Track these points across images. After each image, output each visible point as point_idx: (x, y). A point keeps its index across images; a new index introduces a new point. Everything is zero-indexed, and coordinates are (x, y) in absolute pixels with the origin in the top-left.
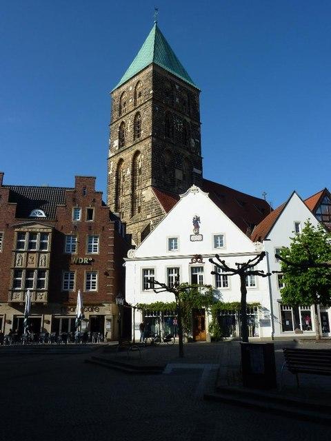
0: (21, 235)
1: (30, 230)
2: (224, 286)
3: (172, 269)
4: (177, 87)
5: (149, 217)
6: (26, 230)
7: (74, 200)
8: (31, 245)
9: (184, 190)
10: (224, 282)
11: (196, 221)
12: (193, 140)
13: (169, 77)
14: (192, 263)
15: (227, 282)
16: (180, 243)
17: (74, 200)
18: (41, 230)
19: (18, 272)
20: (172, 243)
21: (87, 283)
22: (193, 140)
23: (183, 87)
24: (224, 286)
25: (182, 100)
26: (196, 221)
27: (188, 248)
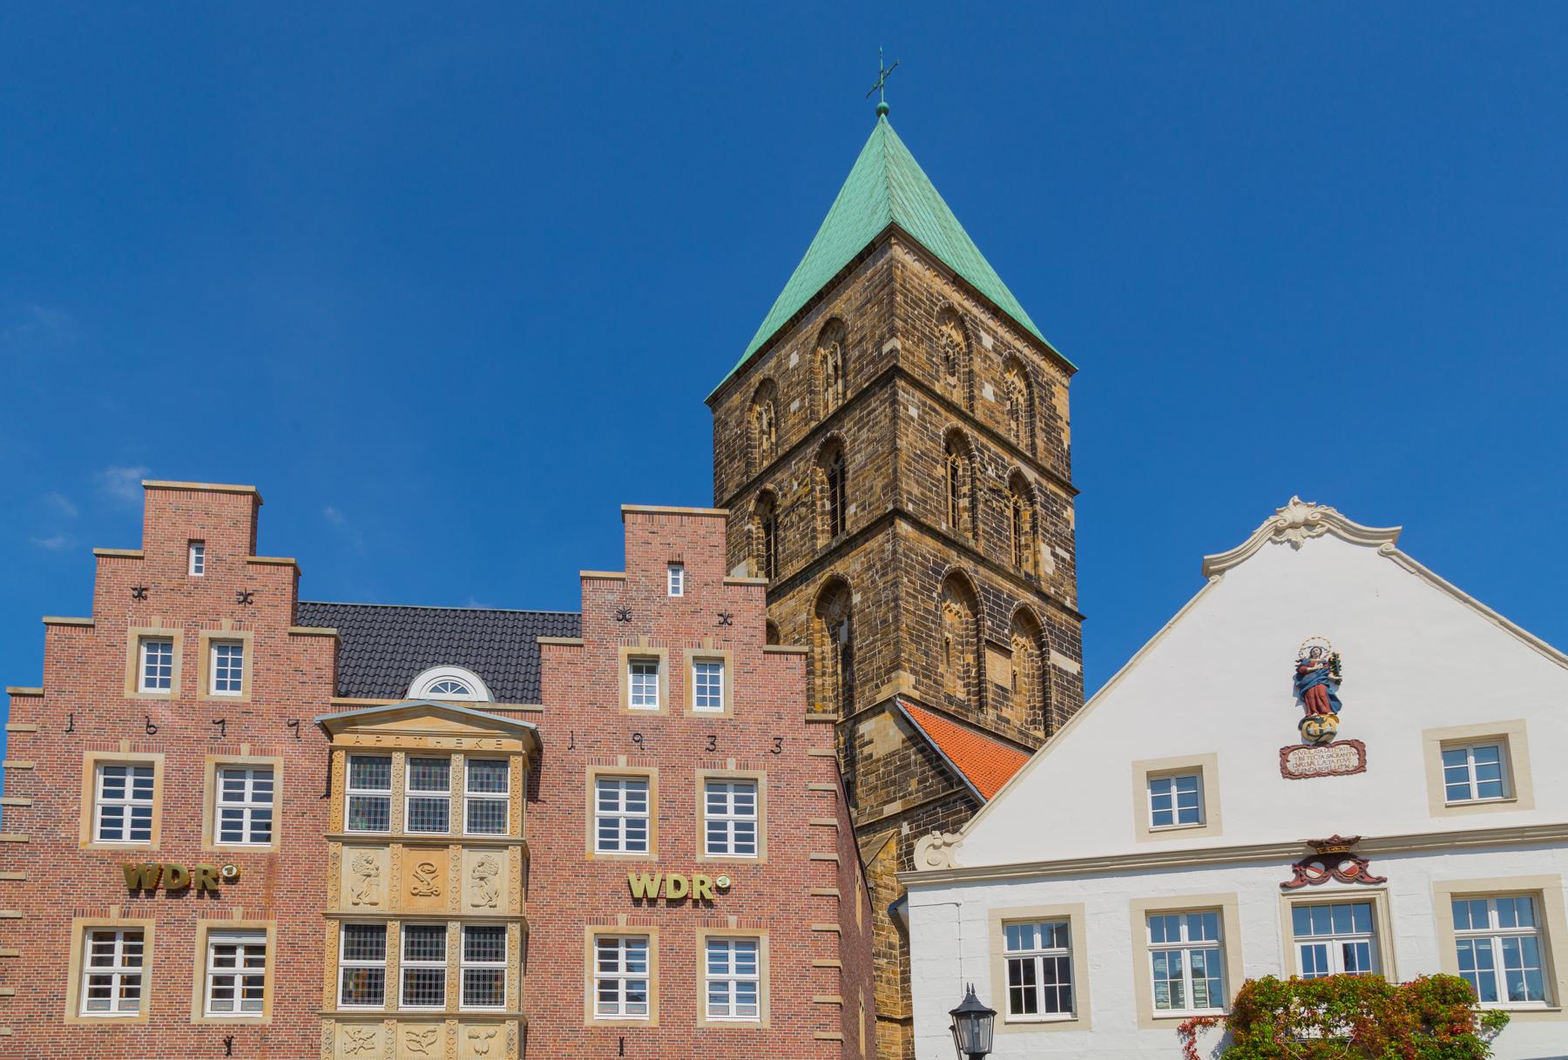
0: (372, 765)
2: (1051, 1007)
3: (1064, 940)
4: (988, 341)
5: (895, 808)
6: (388, 741)
8: (429, 814)
9: (1234, 529)
10: (1030, 979)
11: (1316, 685)
12: (1045, 550)
14: (1302, 879)
15: (1014, 979)
16: (1220, 793)
18: (468, 744)
19: (365, 935)
20: (1178, 790)
21: (604, 984)
22: (1045, 550)
23: (1008, 346)
24: (1051, 1007)
25: (1005, 395)
26: (1316, 685)
27: (1262, 806)
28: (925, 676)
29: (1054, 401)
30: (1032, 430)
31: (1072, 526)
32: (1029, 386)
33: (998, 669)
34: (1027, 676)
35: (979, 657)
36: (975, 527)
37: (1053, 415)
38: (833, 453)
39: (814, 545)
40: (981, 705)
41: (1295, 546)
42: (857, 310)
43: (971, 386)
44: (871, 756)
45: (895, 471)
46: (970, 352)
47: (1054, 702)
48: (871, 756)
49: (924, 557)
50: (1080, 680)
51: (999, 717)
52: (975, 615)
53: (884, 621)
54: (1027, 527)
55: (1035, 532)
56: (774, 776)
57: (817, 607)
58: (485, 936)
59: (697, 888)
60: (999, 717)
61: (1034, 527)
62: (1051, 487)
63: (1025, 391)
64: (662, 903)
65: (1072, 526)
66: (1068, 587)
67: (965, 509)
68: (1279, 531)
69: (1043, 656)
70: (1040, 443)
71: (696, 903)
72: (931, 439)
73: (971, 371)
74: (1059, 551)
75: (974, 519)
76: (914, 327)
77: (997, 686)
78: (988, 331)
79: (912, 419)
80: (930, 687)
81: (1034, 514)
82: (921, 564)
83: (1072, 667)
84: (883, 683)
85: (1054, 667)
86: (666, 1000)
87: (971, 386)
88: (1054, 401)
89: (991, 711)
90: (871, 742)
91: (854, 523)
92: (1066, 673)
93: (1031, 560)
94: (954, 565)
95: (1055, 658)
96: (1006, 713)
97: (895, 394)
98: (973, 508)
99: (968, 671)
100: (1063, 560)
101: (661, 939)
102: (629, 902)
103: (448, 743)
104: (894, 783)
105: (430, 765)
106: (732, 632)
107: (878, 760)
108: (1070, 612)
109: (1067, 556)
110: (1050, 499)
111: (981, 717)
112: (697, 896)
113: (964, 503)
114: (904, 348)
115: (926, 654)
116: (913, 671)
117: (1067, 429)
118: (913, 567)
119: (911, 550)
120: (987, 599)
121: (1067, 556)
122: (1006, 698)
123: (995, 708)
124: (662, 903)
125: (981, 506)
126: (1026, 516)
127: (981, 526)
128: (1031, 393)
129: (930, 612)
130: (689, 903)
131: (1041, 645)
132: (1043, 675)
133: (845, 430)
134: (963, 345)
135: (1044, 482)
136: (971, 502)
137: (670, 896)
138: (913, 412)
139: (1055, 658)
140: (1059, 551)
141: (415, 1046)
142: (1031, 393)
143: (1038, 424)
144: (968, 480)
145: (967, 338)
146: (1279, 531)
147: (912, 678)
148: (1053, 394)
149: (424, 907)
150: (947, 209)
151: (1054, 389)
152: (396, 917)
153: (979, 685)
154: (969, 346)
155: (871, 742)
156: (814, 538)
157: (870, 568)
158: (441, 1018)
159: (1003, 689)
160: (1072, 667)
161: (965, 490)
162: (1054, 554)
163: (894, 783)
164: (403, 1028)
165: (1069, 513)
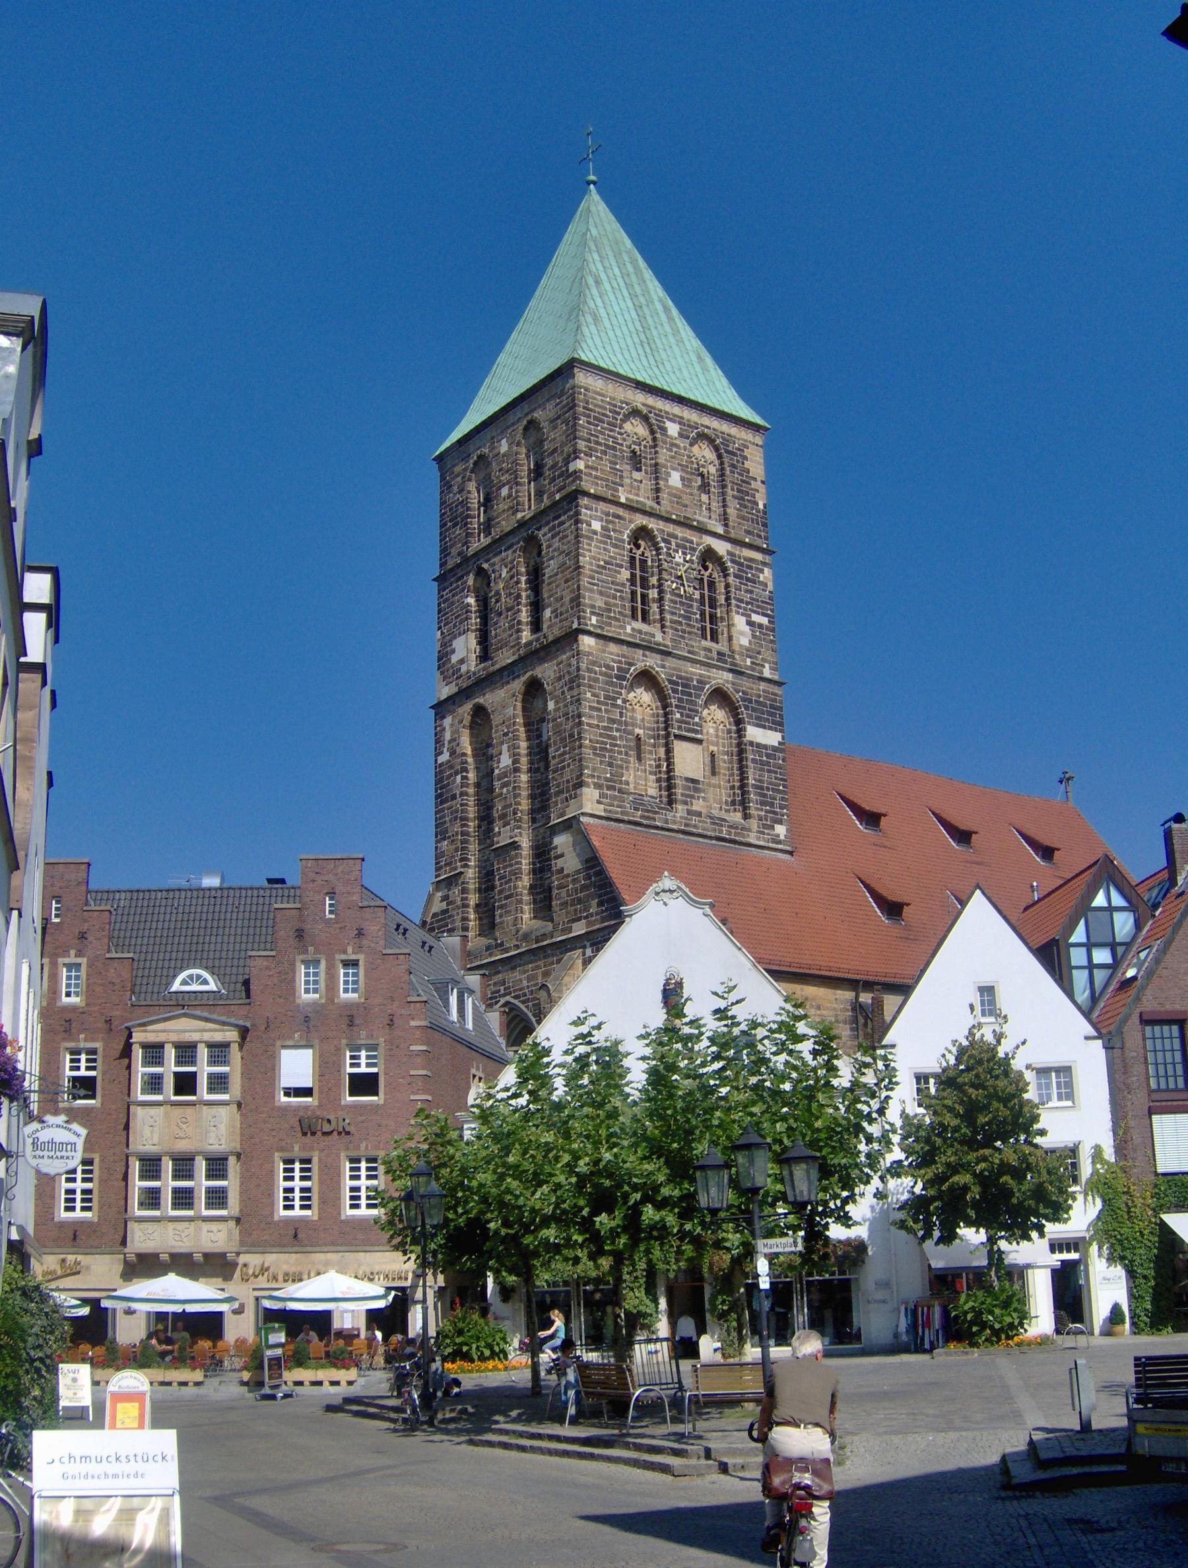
1: (174, 1037)
6: (161, 1038)
7: (300, 934)
12: (740, 622)
13: (640, 399)
17: (300, 934)
18: (207, 1036)
22: (740, 622)
28: (609, 788)
29: (747, 464)
30: (724, 500)
31: (770, 587)
32: (720, 457)
33: (689, 760)
34: (727, 753)
35: (669, 751)
36: (662, 619)
37: (747, 479)
38: (532, 545)
39: (519, 638)
40: (671, 802)
41: (665, 904)
42: (552, 422)
43: (657, 478)
44: (562, 870)
45: (579, 587)
46: (655, 446)
47: (751, 781)
48: (562, 870)
49: (608, 667)
50: (781, 751)
51: (689, 812)
52: (664, 708)
53: (572, 736)
54: (721, 599)
55: (729, 605)
56: (389, 1042)
57: (524, 701)
58: (217, 1166)
59: (341, 1123)
60: (689, 812)
61: (728, 599)
62: (747, 553)
63: (717, 462)
64: (319, 1133)
65: (770, 587)
66: (767, 654)
67: (654, 600)
68: (657, 894)
69: (740, 732)
70: (731, 511)
71: (340, 1133)
72: (615, 546)
73: (656, 464)
74: (756, 618)
75: (662, 612)
76: (597, 443)
77: (688, 780)
78: (514, 748)
79: (595, 533)
80: (614, 798)
81: (727, 586)
82: (605, 675)
83: (771, 738)
84: (571, 798)
85: (751, 744)
86: (323, 1202)
87: (657, 478)
88: (747, 464)
89: (680, 807)
90: (562, 855)
91: (549, 627)
92: (765, 747)
93: (726, 635)
94: (640, 666)
95: (754, 733)
96: (698, 805)
97: (578, 513)
98: (661, 599)
99: (659, 766)
100: (760, 626)
101: (320, 1159)
102: (300, 1135)
103: (195, 1037)
104: (580, 901)
105: (186, 1052)
106: (365, 942)
107: (568, 876)
108: (769, 681)
109: (764, 621)
110: (744, 566)
111: (670, 816)
112: (341, 1129)
113: (653, 594)
114: (587, 467)
115: (610, 765)
116: (598, 786)
117: (762, 489)
118: (596, 680)
119: (594, 663)
120: (675, 691)
121: (764, 621)
122: (697, 790)
123: (686, 803)
124: (319, 1133)
125: (668, 596)
126: (721, 588)
127: (668, 617)
128: (722, 464)
129: (613, 721)
130: (335, 1133)
131: (738, 722)
132: (741, 749)
133: (543, 535)
134: (649, 438)
135: (737, 551)
136: (660, 593)
137: (325, 1130)
138: (596, 526)
139: (754, 733)
140: (756, 618)
141: (177, 1238)
142: (722, 464)
143: (730, 492)
144: (656, 570)
145: (652, 432)
146: (657, 894)
147: (596, 794)
148: (746, 458)
149: (183, 1146)
150: (648, 274)
151: (746, 452)
152: (166, 1154)
153: (668, 782)
154: (654, 439)
155: (562, 855)
156: (519, 631)
157: (559, 679)
158: (190, 1219)
159: (693, 781)
160: (771, 738)
161: (654, 580)
162: (750, 623)
163: (580, 901)
164: (171, 1226)
165: (766, 575)
